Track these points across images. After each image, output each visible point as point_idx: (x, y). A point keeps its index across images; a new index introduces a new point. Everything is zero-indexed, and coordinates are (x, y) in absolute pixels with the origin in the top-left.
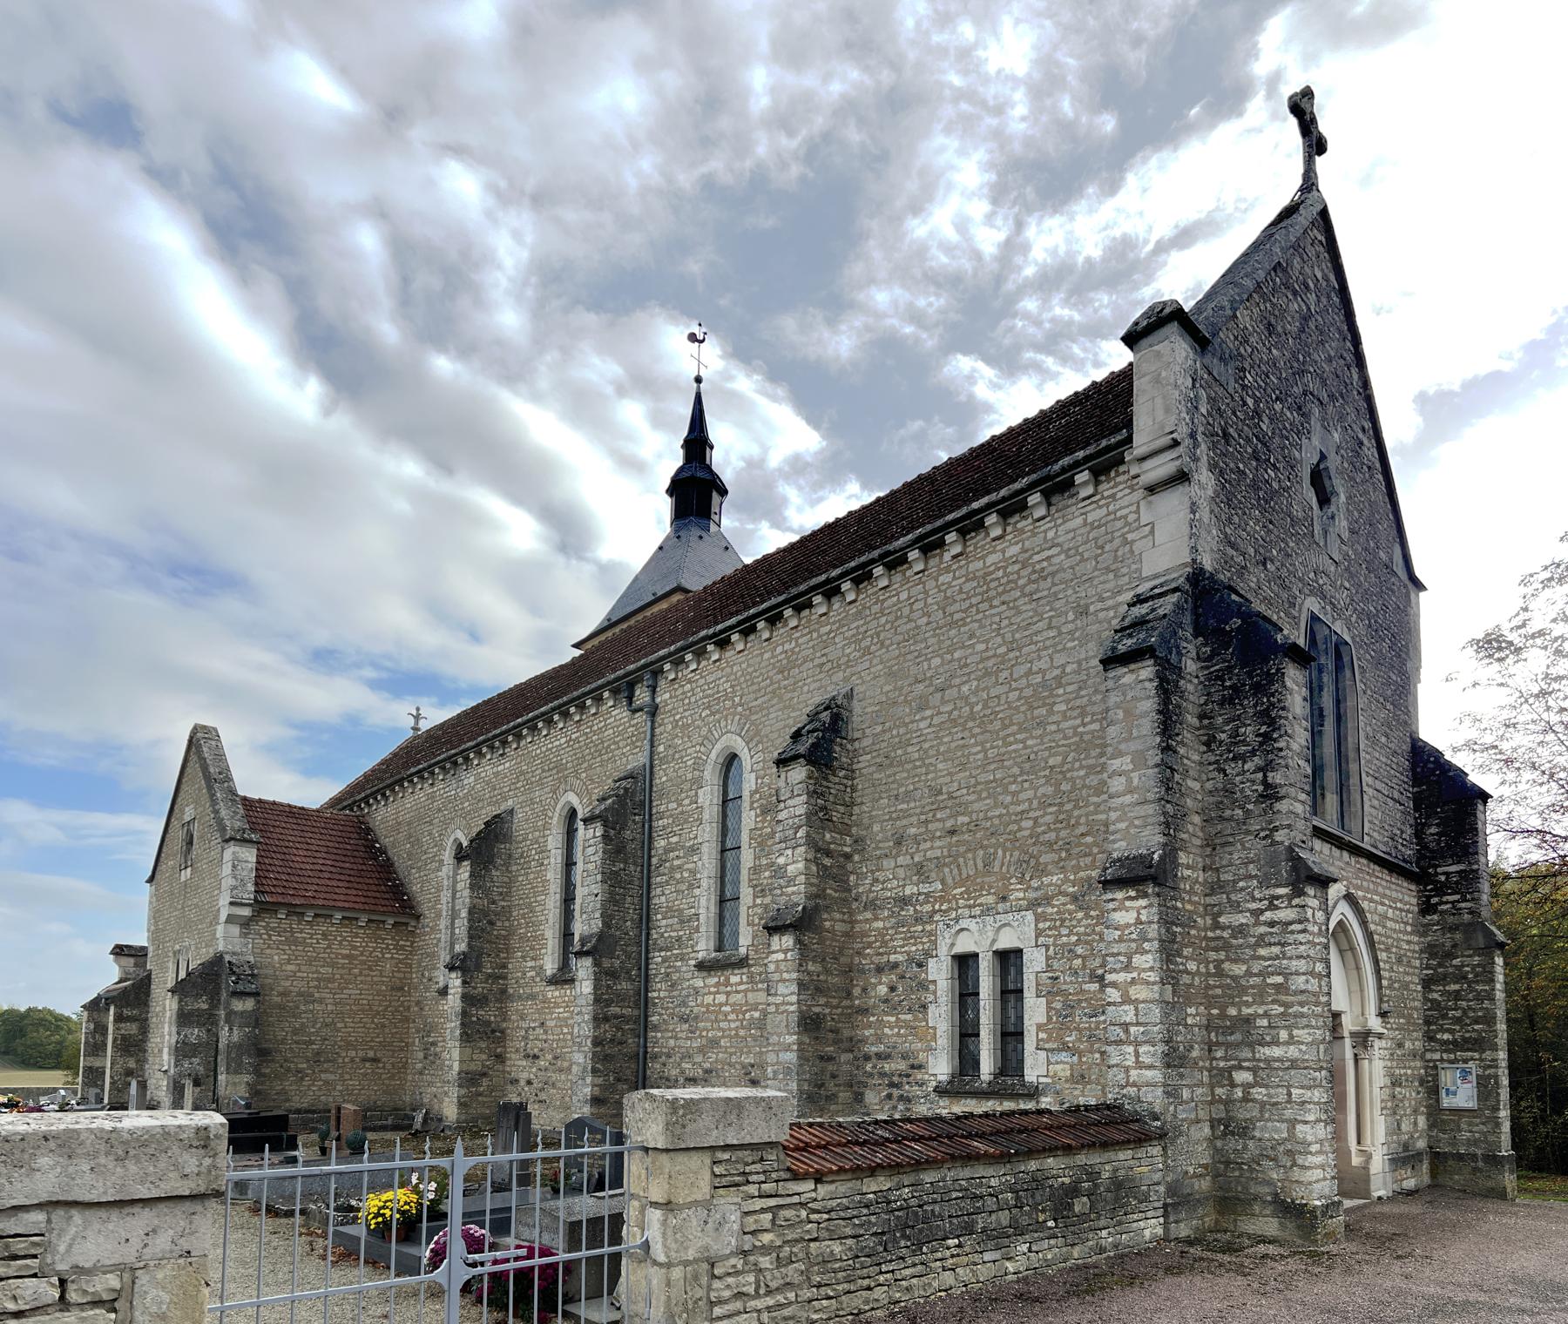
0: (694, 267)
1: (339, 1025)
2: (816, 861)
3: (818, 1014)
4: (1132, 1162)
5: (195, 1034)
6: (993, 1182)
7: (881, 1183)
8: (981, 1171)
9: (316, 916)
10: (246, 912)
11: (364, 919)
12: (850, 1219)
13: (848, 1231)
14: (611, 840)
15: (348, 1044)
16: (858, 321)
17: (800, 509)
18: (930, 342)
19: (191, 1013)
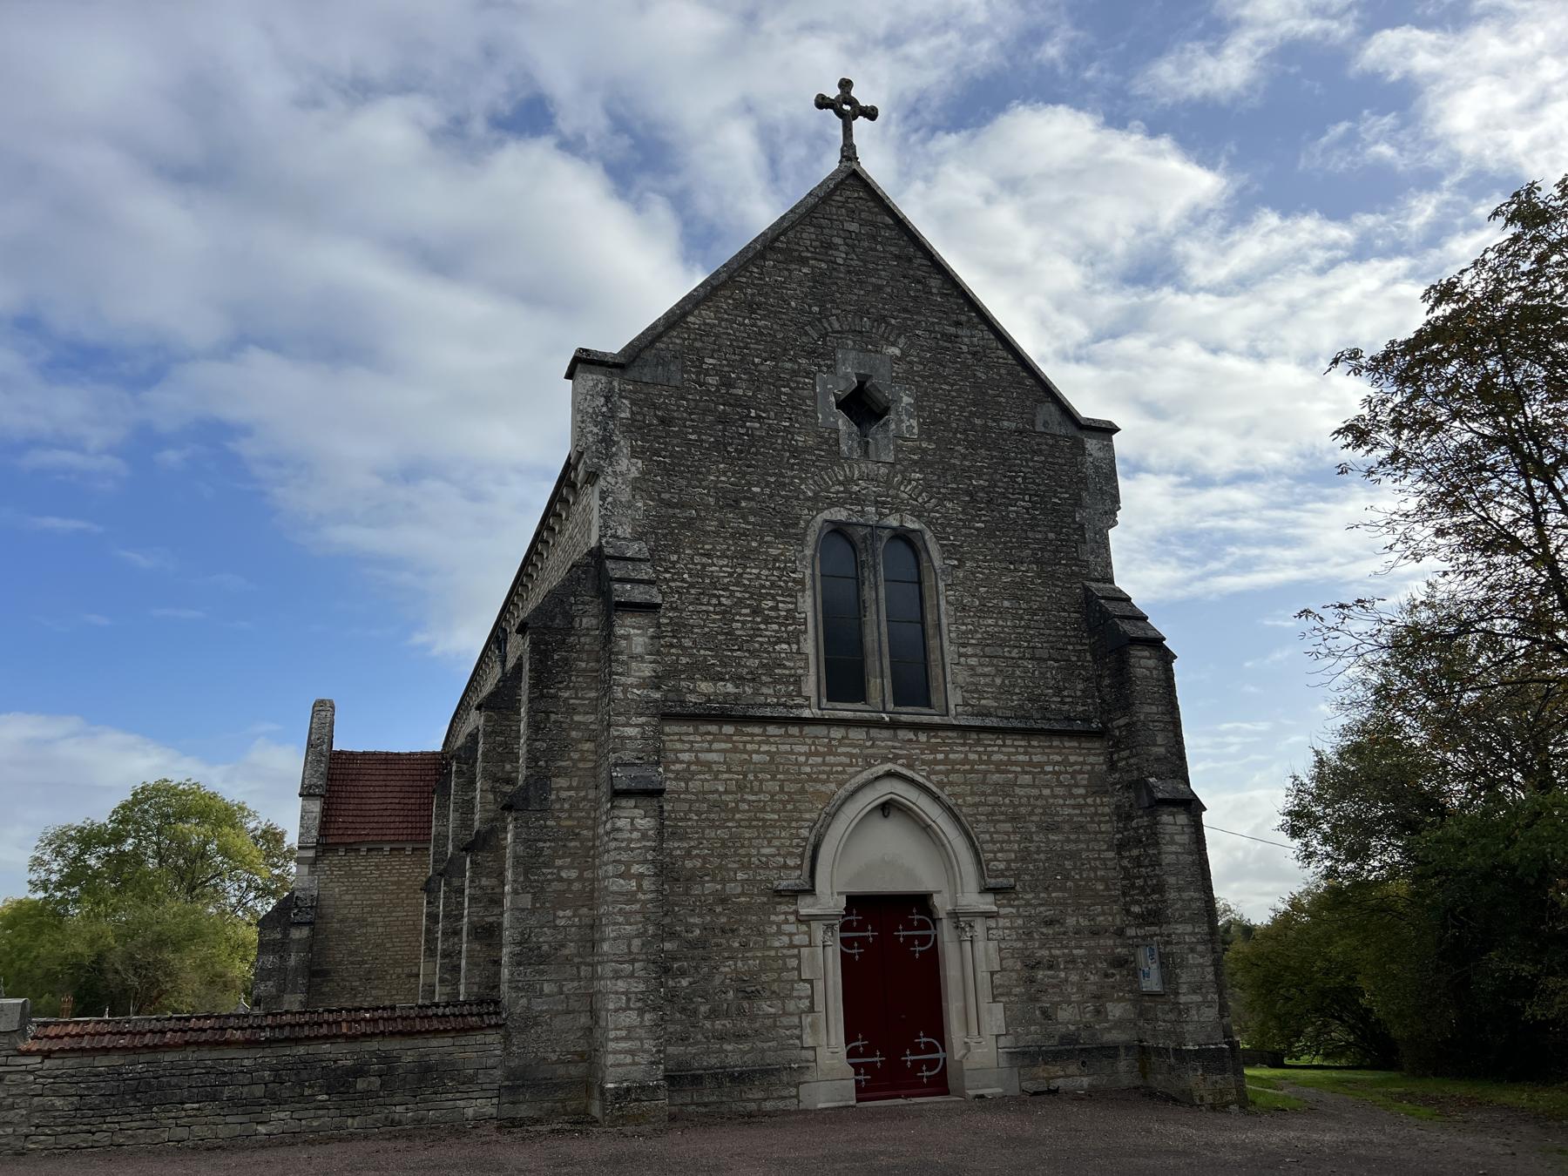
0: (1052, 51)
1: (388, 945)
2: (493, 790)
3: (491, 924)
4: (451, 1049)
5: (270, 960)
6: (246, 1062)
7: (115, 1060)
8: (232, 1053)
9: (369, 850)
10: (311, 854)
11: (409, 848)
12: (77, 1083)
13: (72, 1091)
14: (464, 774)
15: (396, 961)
16: (1245, 39)
17: (1208, 265)
18: (1342, 31)
19: (268, 943)
